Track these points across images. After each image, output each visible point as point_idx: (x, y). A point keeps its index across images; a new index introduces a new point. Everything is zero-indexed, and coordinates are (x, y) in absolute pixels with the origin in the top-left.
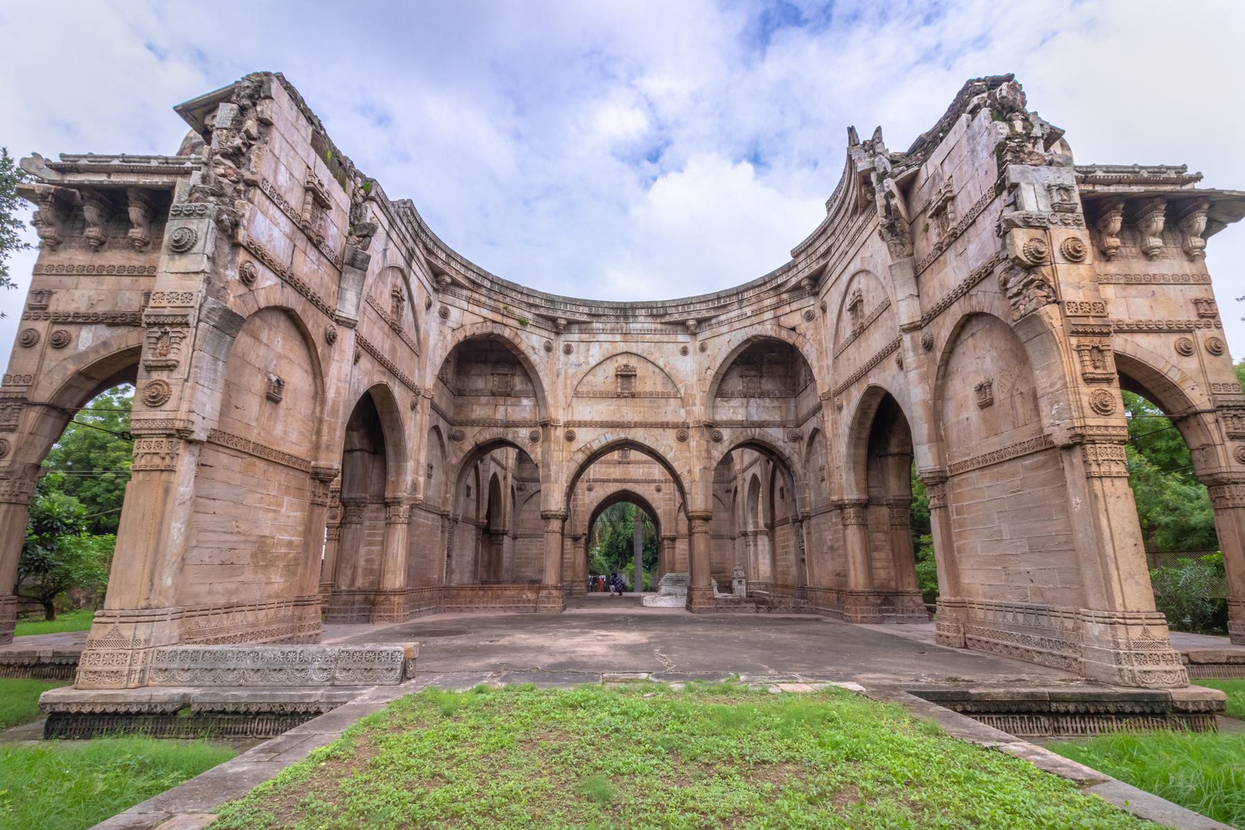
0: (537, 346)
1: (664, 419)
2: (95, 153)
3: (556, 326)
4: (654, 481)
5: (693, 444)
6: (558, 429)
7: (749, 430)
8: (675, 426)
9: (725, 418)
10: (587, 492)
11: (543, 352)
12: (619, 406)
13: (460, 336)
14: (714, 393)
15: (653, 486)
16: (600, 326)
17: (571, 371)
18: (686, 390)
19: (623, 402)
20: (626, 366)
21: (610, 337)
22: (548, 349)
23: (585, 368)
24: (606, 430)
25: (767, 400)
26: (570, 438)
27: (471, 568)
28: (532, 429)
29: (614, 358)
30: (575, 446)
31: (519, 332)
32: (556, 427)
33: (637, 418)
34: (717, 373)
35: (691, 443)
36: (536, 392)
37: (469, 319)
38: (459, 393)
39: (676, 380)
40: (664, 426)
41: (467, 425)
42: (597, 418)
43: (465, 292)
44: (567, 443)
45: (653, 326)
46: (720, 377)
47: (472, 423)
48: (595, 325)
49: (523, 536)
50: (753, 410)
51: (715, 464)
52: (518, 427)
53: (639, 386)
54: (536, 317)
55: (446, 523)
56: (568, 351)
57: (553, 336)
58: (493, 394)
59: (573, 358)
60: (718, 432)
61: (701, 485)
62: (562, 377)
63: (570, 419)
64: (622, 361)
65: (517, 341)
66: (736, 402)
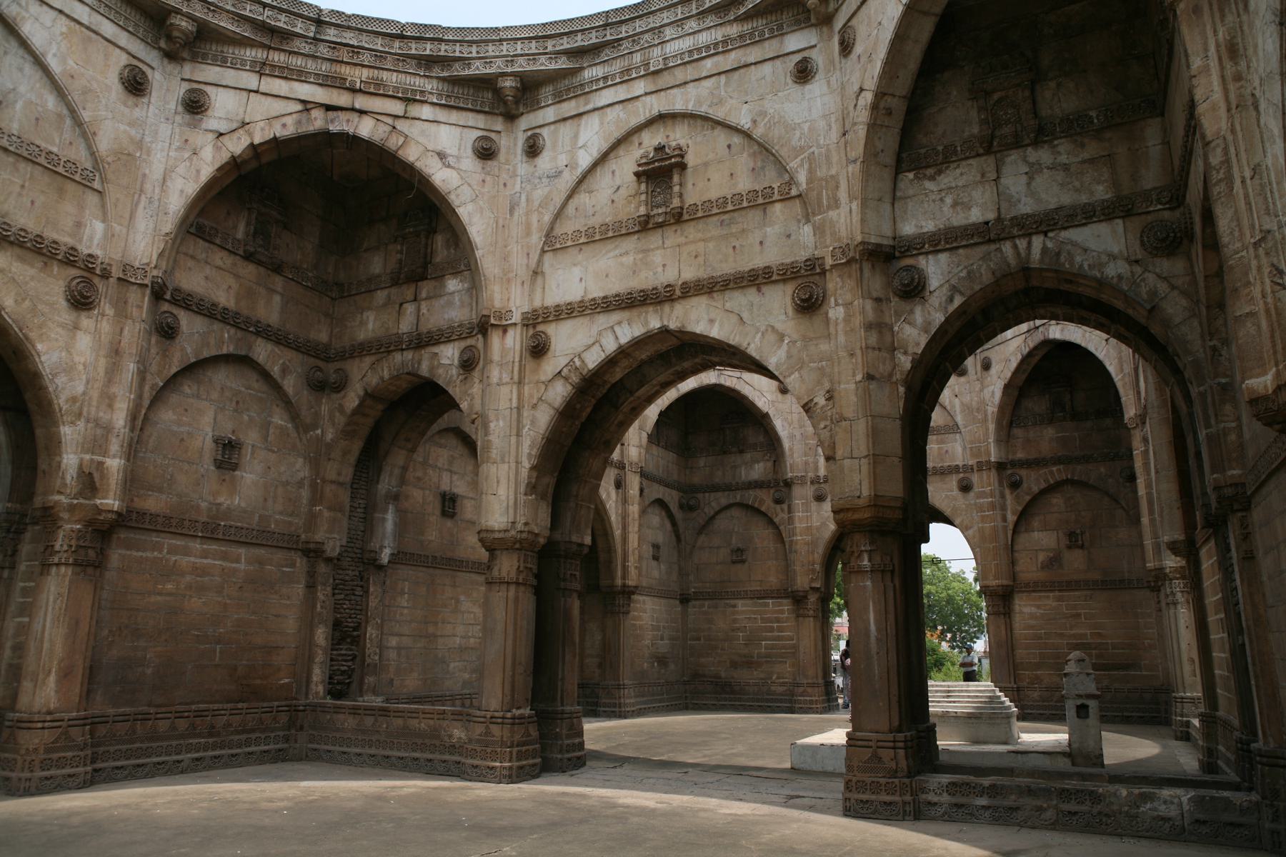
0: (451, 150)
1: (758, 262)
4: (956, 469)
5: (836, 312)
6: (511, 333)
7: (1007, 248)
8: (787, 274)
9: (929, 226)
10: (814, 505)
11: (469, 162)
12: (646, 251)
13: (237, 145)
14: (889, 159)
15: (953, 481)
16: (598, 72)
17: (539, 194)
18: (811, 171)
19: (654, 239)
20: (660, 149)
21: (621, 93)
22: (486, 152)
23: (569, 179)
24: (615, 317)
25: (1064, 146)
26: (538, 350)
28: (463, 344)
29: (635, 139)
30: (550, 366)
31: (401, 125)
32: (505, 329)
33: (689, 274)
34: (880, 95)
35: (832, 314)
37: (260, 109)
39: (784, 152)
40: (757, 279)
41: (352, 357)
42: (596, 292)
43: (250, 54)
44: (530, 364)
45: (718, 35)
46: (898, 106)
47: (362, 350)
48: (588, 74)
49: (699, 596)
50: (1014, 181)
51: (905, 362)
52: (438, 343)
54: (446, 87)
55: (322, 568)
57: (498, 124)
58: (396, 282)
59: (545, 162)
60: (908, 268)
61: (861, 427)
62: (520, 211)
63: (537, 303)
64: (650, 140)
65: (393, 143)
66: (960, 176)
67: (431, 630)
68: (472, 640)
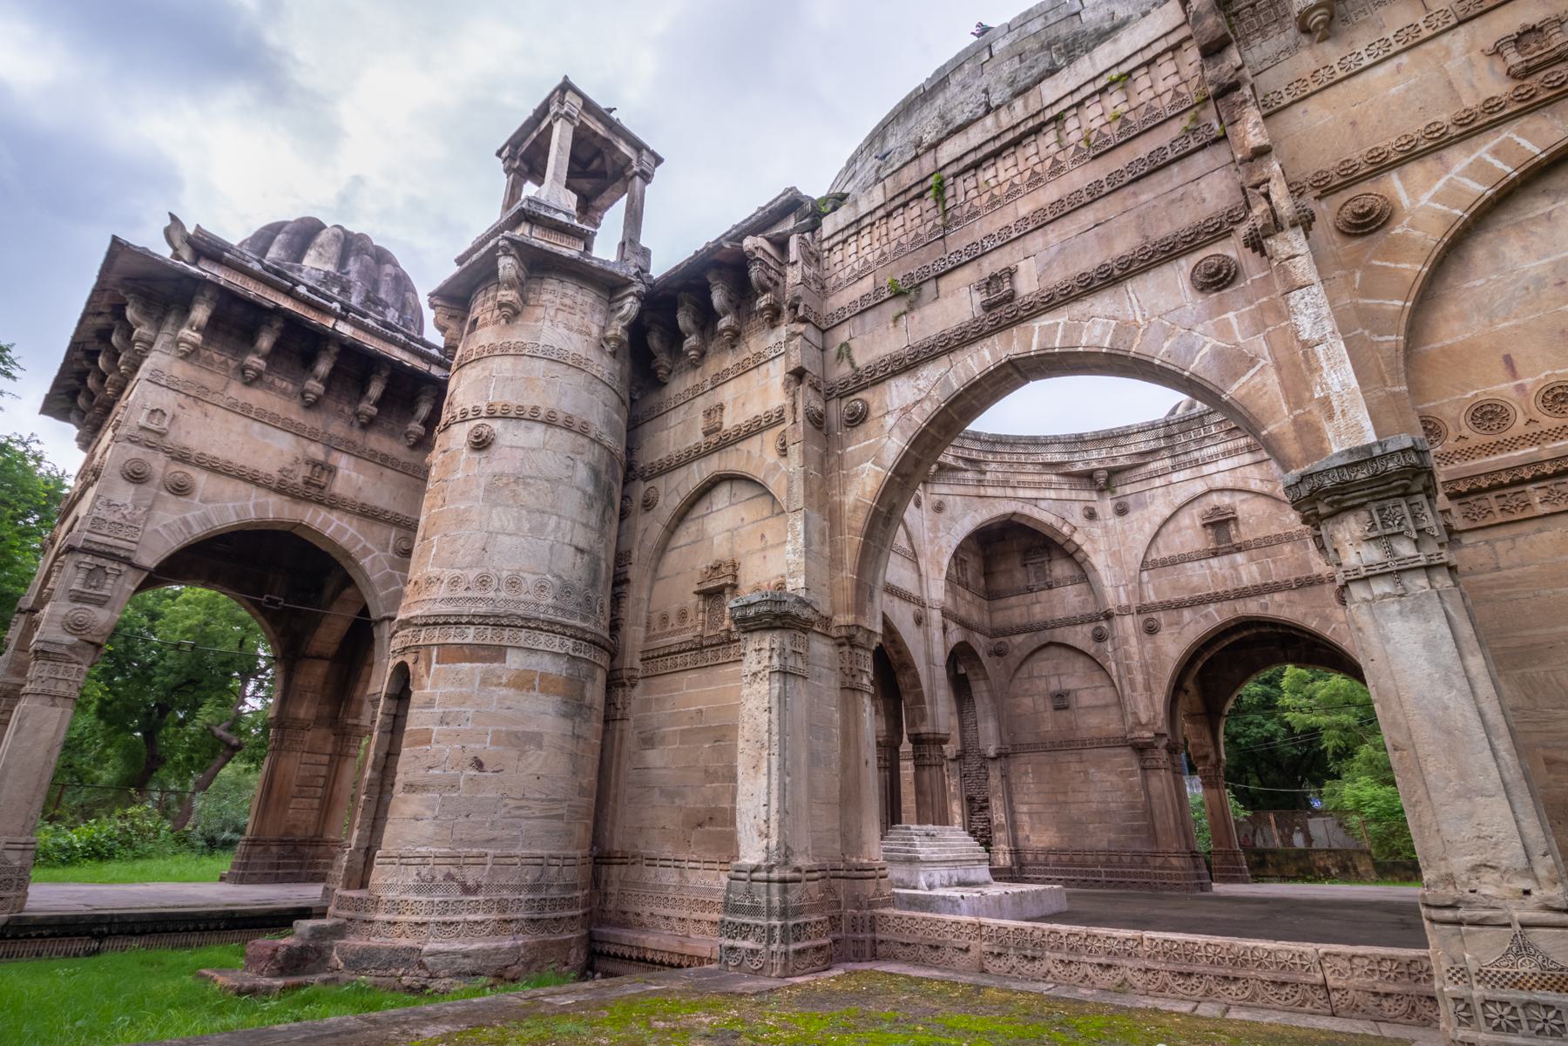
2: (763, 205)
3: (1102, 481)
27: (1474, 638)
36: (1083, 573)
38: (992, 596)
53: (1244, 533)
56: (1122, 511)
57: (1095, 496)
67: (1061, 798)
68: (1112, 805)
